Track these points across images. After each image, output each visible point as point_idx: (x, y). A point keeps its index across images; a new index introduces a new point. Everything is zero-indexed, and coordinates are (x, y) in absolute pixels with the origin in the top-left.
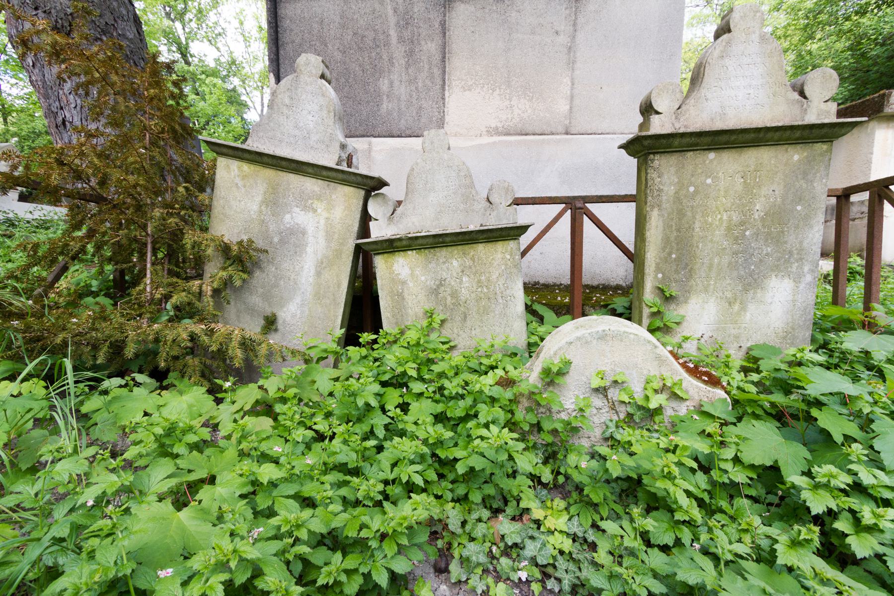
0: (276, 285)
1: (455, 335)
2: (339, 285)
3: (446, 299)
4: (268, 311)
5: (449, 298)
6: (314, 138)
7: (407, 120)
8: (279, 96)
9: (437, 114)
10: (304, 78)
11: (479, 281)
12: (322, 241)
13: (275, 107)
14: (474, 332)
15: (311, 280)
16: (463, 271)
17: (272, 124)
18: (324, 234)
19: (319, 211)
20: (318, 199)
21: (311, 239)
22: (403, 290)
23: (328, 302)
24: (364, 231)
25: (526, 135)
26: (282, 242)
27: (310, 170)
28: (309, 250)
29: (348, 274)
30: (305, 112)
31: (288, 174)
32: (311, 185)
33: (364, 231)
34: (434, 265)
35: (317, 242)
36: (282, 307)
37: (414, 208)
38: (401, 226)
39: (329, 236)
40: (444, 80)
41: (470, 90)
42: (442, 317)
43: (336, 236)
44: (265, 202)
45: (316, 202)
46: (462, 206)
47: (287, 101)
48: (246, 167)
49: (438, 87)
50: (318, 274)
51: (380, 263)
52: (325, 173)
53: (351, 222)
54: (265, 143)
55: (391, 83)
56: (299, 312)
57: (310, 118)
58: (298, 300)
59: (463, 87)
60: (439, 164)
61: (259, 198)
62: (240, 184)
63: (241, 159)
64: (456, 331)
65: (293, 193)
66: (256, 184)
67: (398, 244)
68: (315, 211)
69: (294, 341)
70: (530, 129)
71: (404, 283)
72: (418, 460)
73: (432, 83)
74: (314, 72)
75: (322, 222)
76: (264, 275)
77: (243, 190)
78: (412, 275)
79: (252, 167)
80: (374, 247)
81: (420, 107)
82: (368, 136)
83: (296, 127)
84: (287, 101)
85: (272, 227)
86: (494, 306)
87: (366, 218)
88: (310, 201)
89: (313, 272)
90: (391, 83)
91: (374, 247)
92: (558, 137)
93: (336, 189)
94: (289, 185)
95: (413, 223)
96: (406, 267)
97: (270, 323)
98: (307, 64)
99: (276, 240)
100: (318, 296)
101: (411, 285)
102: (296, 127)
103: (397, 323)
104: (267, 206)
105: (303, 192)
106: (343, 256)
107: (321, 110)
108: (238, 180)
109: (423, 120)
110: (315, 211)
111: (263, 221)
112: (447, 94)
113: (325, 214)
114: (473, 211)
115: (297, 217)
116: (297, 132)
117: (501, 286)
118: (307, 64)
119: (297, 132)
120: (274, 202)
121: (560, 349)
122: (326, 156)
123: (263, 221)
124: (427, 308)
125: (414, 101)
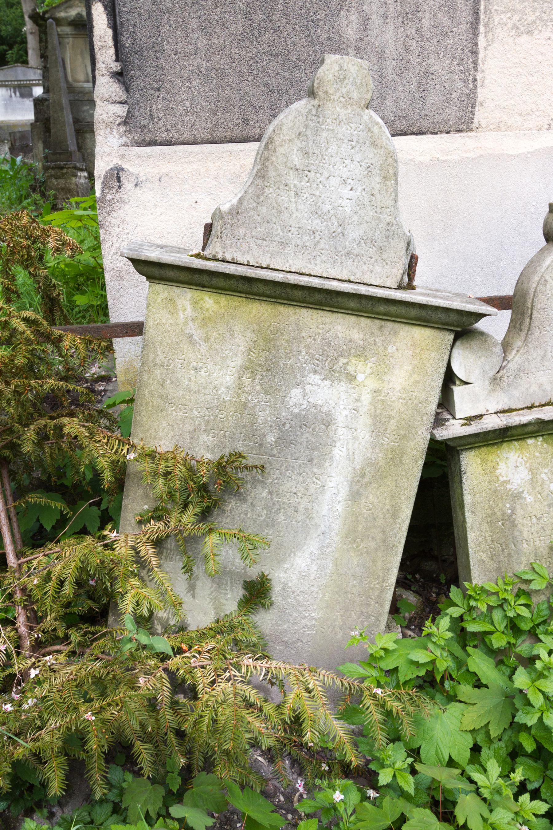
0: (271, 524)
2: (395, 515)
4: (253, 573)
6: (353, 233)
7: (397, 100)
8: (281, 150)
9: (460, 84)
10: (334, 109)
12: (364, 435)
13: (272, 173)
15: (340, 508)
17: (264, 210)
18: (369, 421)
19: (360, 377)
20: (358, 356)
21: (342, 433)
22: (513, 509)
23: (372, 545)
26: (284, 441)
27: (352, 304)
28: (338, 452)
30: (334, 182)
31: (298, 310)
32: (344, 328)
35: (355, 438)
36: (280, 561)
37: (544, 358)
38: (516, 393)
39: (378, 424)
40: (476, 14)
41: (529, 33)
43: (393, 424)
44: (249, 368)
45: (354, 361)
47: (297, 159)
48: (210, 301)
49: (464, 27)
50: (355, 496)
51: (471, 463)
52: (382, 308)
53: (423, 397)
54: (250, 250)
55: (365, 22)
56: (314, 568)
57: (345, 192)
58: (312, 546)
59: (515, 27)
61: (237, 361)
62: (197, 334)
63: (202, 286)
65: (308, 347)
66: (232, 333)
68: (351, 378)
69: (304, 621)
71: (516, 497)
72: (188, 467)
73: (452, 19)
74: (355, 95)
75: (366, 398)
76: (245, 507)
77: (204, 347)
78: (533, 482)
79: (224, 300)
80: (463, 442)
81: (427, 72)
83: (316, 212)
84: (297, 159)
85: (263, 415)
88: (342, 361)
89: (344, 492)
90: (365, 22)
93: (395, 334)
94: (300, 330)
95: (540, 386)
96: (522, 468)
97: (257, 593)
98: (341, 79)
99: (271, 439)
100: (352, 536)
101: (529, 499)
102: (316, 212)
103: (498, 569)
104: (254, 374)
105: (329, 344)
106: (406, 459)
107: (369, 175)
108: (193, 329)
109: (432, 99)
110: (351, 378)
111: (245, 405)
112: (482, 41)
113: (372, 384)
115: (318, 392)
116: (317, 224)
118: (341, 79)
119: (317, 224)
120: (268, 366)
122: (378, 269)
123: (245, 405)
125: (414, 60)
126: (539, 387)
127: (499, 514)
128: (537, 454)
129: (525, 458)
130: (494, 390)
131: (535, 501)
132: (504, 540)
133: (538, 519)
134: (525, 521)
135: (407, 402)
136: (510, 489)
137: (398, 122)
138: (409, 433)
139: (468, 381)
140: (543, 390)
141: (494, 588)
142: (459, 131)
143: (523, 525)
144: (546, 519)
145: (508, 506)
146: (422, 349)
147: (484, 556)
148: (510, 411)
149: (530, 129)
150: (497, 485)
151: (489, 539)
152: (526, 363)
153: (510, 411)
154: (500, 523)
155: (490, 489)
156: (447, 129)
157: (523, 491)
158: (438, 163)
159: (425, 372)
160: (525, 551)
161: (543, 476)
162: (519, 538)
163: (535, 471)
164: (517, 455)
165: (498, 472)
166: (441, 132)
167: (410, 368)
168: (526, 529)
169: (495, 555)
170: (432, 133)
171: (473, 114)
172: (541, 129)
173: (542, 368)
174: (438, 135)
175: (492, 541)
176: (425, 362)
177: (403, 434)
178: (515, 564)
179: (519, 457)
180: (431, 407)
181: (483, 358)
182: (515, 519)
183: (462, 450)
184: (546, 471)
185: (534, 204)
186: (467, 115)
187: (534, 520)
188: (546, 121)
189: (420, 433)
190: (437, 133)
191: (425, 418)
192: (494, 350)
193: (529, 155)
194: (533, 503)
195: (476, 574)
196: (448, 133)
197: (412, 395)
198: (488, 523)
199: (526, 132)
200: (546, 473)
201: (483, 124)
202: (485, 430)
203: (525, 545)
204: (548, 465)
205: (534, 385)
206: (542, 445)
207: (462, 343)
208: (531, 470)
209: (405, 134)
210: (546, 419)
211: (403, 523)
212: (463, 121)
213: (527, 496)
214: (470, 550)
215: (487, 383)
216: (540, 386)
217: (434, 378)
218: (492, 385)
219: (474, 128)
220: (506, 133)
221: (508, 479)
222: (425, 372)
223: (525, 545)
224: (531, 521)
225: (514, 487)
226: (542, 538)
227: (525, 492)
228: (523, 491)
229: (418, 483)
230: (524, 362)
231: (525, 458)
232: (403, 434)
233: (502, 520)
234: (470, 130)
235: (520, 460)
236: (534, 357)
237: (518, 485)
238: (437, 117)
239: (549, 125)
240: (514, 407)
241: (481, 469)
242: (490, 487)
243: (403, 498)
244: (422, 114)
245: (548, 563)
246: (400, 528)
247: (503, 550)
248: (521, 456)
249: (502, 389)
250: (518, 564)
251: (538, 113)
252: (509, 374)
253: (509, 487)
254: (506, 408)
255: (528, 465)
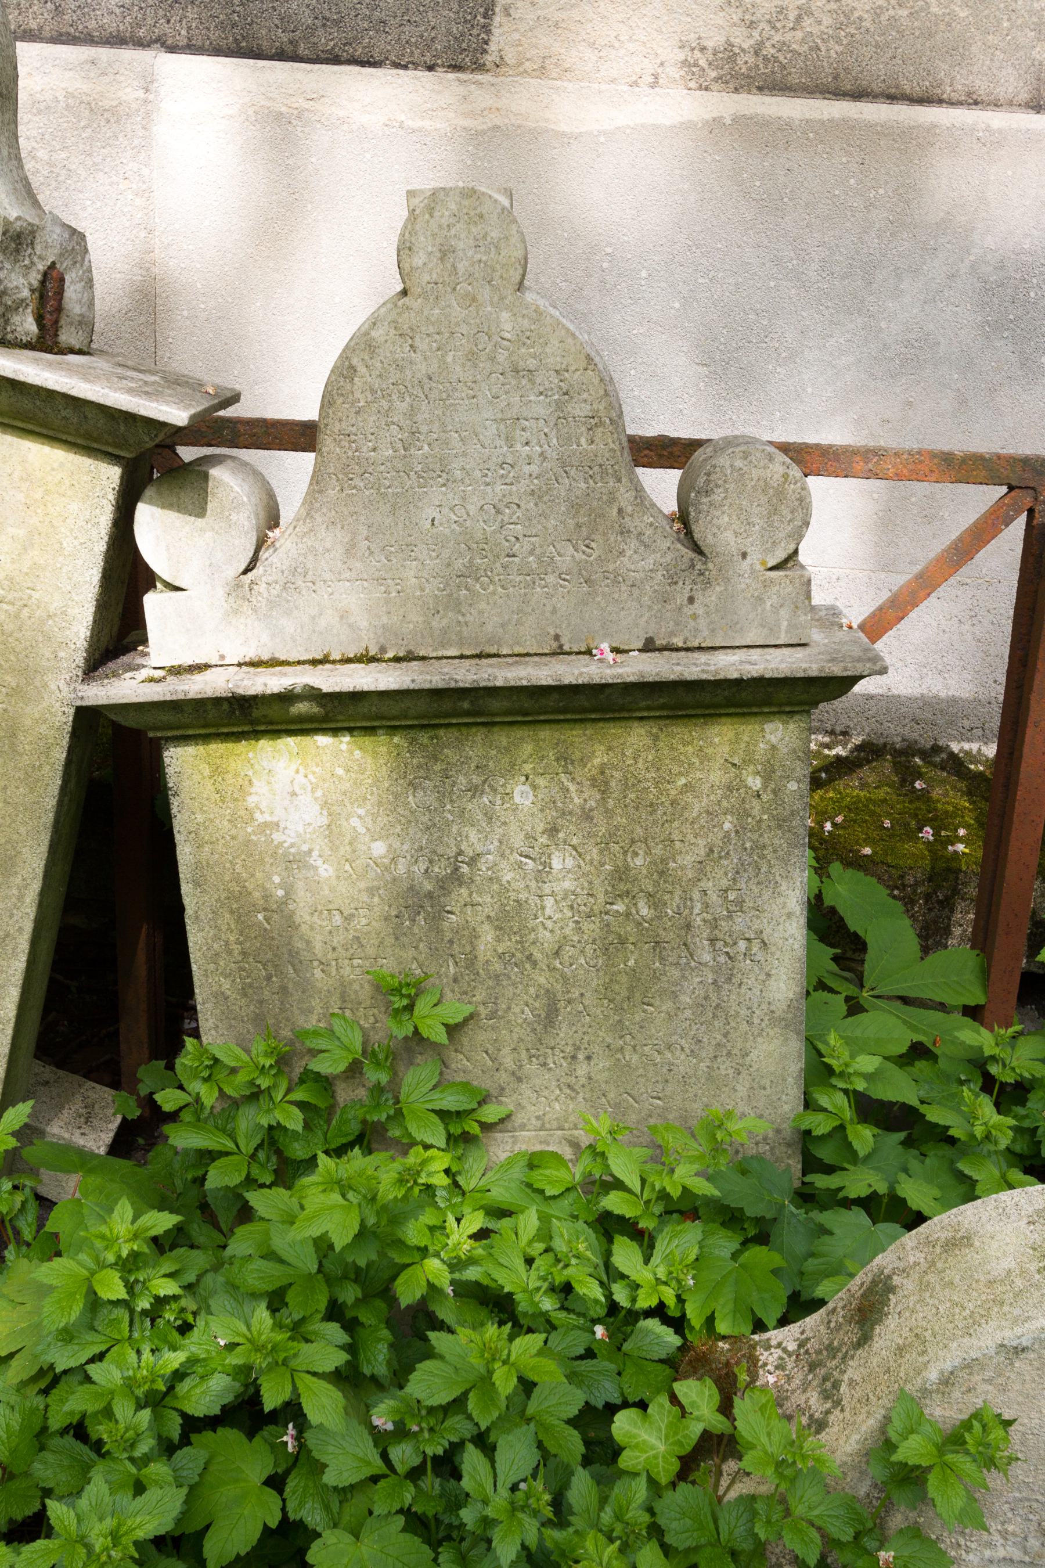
1: (503, 1077)
3: (475, 935)
5: (487, 936)
11: (621, 874)
14: (582, 1069)
16: (553, 831)
24: (119, 629)
25: (859, 95)
29: (49, 818)
33: (119, 629)
34: (431, 799)
42: (455, 1011)
46: (568, 556)
60: (472, 357)
64: (508, 1062)
67: (274, 711)
70: (877, 71)
78: (332, 831)
80: (166, 717)
82: (141, 44)
86: (675, 973)
87: (127, 579)
91: (166, 717)
92: (997, 119)
103: (258, 1019)
114: (616, 579)
117: (714, 897)
121: (969, 1366)
124: (388, 965)
126: (342, 617)
127: (257, 895)
128: (340, 772)
129: (310, 776)
130: (236, 612)
131: (338, 877)
132: (270, 955)
133: (348, 919)
134: (315, 918)
135: (20, 611)
136: (281, 844)
137: (320, 32)
138: (28, 684)
139: (177, 584)
140: (350, 626)
141: (237, 1058)
142: (456, 68)
143: (312, 928)
144: (364, 921)
145: (277, 879)
146: (47, 492)
147: (226, 985)
148: (274, 663)
149: (613, 81)
150: (249, 830)
151: (236, 948)
152: (310, 557)
153: (274, 663)
154: (260, 916)
155: (233, 838)
156: (428, 58)
157: (310, 851)
158: (401, 132)
159: (57, 546)
160: (319, 985)
161: (355, 822)
162: (305, 955)
163: (335, 809)
164: (294, 767)
165: (251, 801)
166: (416, 66)
167: (21, 532)
168: (319, 937)
169: (251, 986)
170: (397, 65)
171: (489, 32)
172: (635, 84)
173: (348, 575)
174: (409, 72)
175: (244, 954)
176: (55, 522)
177: (14, 684)
178: (297, 1012)
179: (297, 772)
180: (74, 629)
181: (209, 535)
182: (293, 912)
183: (168, 739)
184: (361, 812)
185: (609, 250)
186: (475, 32)
187: (338, 919)
188: (650, 66)
189: (53, 687)
190: (405, 67)
191: (62, 654)
192: (234, 517)
193: (602, 139)
194: (334, 882)
195: (210, 1023)
196: (431, 68)
197: (30, 597)
198: (232, 912)
199: (603, 87)
200: (360, 817)
201: (510, 58)
202: (181, 697)
203: (318, 973)
204: (365, 799)
205: (329, 612)
206: (351, 753)
207: (159, 493)
208: (325, 805)
209: (336, 60)
210: (326, 689)
211: (26, 887)
212: (464, 45)
213: (319, 863)
214: (194, 967)
215: (221, 592)
216: (344, 615)
217: (80, 562)
218: (231, 600)
219: (489, 65)
220: (558, 83)
221: (275, 819)
222: (57, 546)
223: (318, 973)
224: (330, 920)
225: (290, 841)
226: (356, 962)
227: (316, 853)
228: (310, 851)
229: (54, 802)
230: (305, 556)
231: (310, 776)
232: (14, 684)
233: (265, 909)
234: (479, 67)
235: (300, 779)
236: (328, 545)
237: (299, 835)
238: (407, 28)
239: (656, 76)
240: (282, 658)
241: (212, 788)
242: (233, 832)
243: (23, 830)
244: (374, 18)
245: (372, 1020)
246: (21, 898)
247: (269, 978)
248: (302, 770)
249: (255, 610)
250: (303, 1012)
251: (631, 46)
252: (270, 579)
253: (277, 837)
254: (265, 657)
255: (319, 793)
